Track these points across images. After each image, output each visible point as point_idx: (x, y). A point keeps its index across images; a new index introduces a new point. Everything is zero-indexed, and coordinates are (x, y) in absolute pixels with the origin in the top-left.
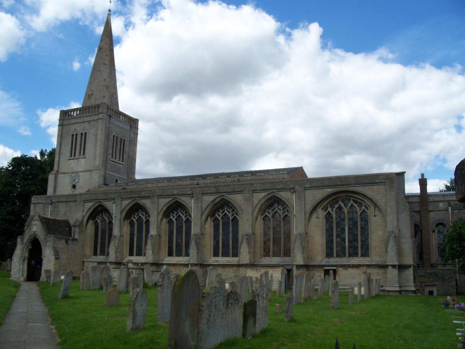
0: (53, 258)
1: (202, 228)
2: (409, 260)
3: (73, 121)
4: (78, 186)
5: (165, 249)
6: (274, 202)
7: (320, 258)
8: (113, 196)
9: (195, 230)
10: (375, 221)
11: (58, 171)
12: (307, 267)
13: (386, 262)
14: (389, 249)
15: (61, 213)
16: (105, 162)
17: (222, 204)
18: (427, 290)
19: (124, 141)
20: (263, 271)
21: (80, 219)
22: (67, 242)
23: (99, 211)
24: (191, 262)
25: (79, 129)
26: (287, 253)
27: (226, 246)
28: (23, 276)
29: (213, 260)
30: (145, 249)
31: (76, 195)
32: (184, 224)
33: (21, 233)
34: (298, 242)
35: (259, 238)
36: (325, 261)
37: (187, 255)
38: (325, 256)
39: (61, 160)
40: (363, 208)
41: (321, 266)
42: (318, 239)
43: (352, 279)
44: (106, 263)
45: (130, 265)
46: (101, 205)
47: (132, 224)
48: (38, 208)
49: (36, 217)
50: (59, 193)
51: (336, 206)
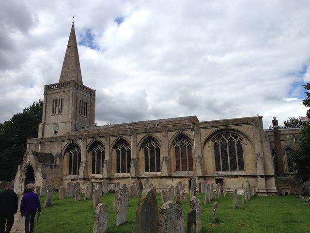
0: (41, 178)
1: (138, 155)
2: (271, 172)
3: (54, 91)
4: (58, 131)
5: (173, 167)
6: (181, 137)
7: (211, 171)
9: (133, 156)
10: (247, 148)
11: (45, 123)
12: (204, 177)
13: (256, 173)
14: (258, 165)
16: (75, 117)
17: (149, 139)
18: (283, 192)
20: (178, 181)
22: (51, 168)
23: (72, 147)
25: (57, 96)
26: (191, 169)
27: (123, 167)
29: (117, 175)
30: (102, 169)
31: (57, 137)
32: (126, 153)
33: (21, 162)
34: (198, 161)
35: (173, 160)
36: (216, 174)
37: (129, 171)
38: (215, 170)
39: (46, 116)
40: (238, 139)
41: (213, 177)
42: (210, 160)
43: (236, 185)
44: (77, 179)
45: (93, 180)
46: (73, 143)
47: (94, 154)
48: (31, 146)
49: (30, 152)
50: (46, 136)
51: (221, 139)
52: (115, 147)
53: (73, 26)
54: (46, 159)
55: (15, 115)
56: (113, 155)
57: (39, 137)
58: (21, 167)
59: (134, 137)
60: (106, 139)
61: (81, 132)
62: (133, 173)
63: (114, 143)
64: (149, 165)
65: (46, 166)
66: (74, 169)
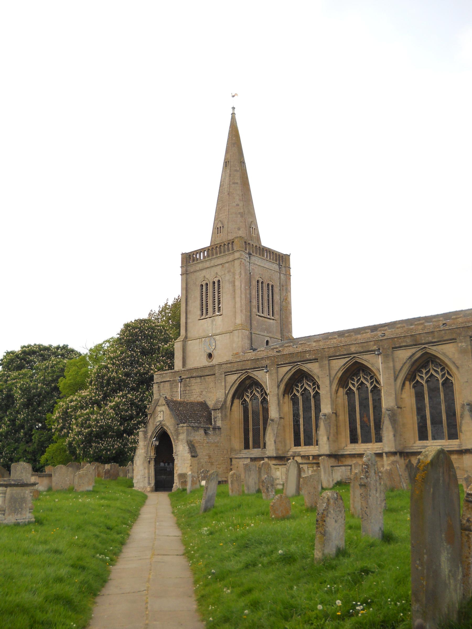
0: (188, 456)
1: (398, 399)
3: (200, 266)
4: (215, 354)
8: (265, 363)
9: (387, 402)
15: (198, 393)
19: (272, 286)
21: (222, 399)
22: (206, 433)
23: (247, 386)
24: (387, 450)
25: (209, 276)
27: (365, 426)
28: (149, 484)
31: (213, 366)
37: (379, 439)
39: (189, 321)
45: (299, 459)
46: (249, 378)
47: (295, 401)
48: (163, 390)
49: (162, 401)
52: (343, 381)
53: (233, 114)
54: (197, 415)
55: (127, 326)
56: (340, 401)
57: (176, 368)
58: (145, 433)
59: (386, 357)
60: (321, 367)
61: (262, 352)
62: (388, 443)
63: (340, 375)
64: (429, 422)
65: (196, 429)
66: (253, 434)
